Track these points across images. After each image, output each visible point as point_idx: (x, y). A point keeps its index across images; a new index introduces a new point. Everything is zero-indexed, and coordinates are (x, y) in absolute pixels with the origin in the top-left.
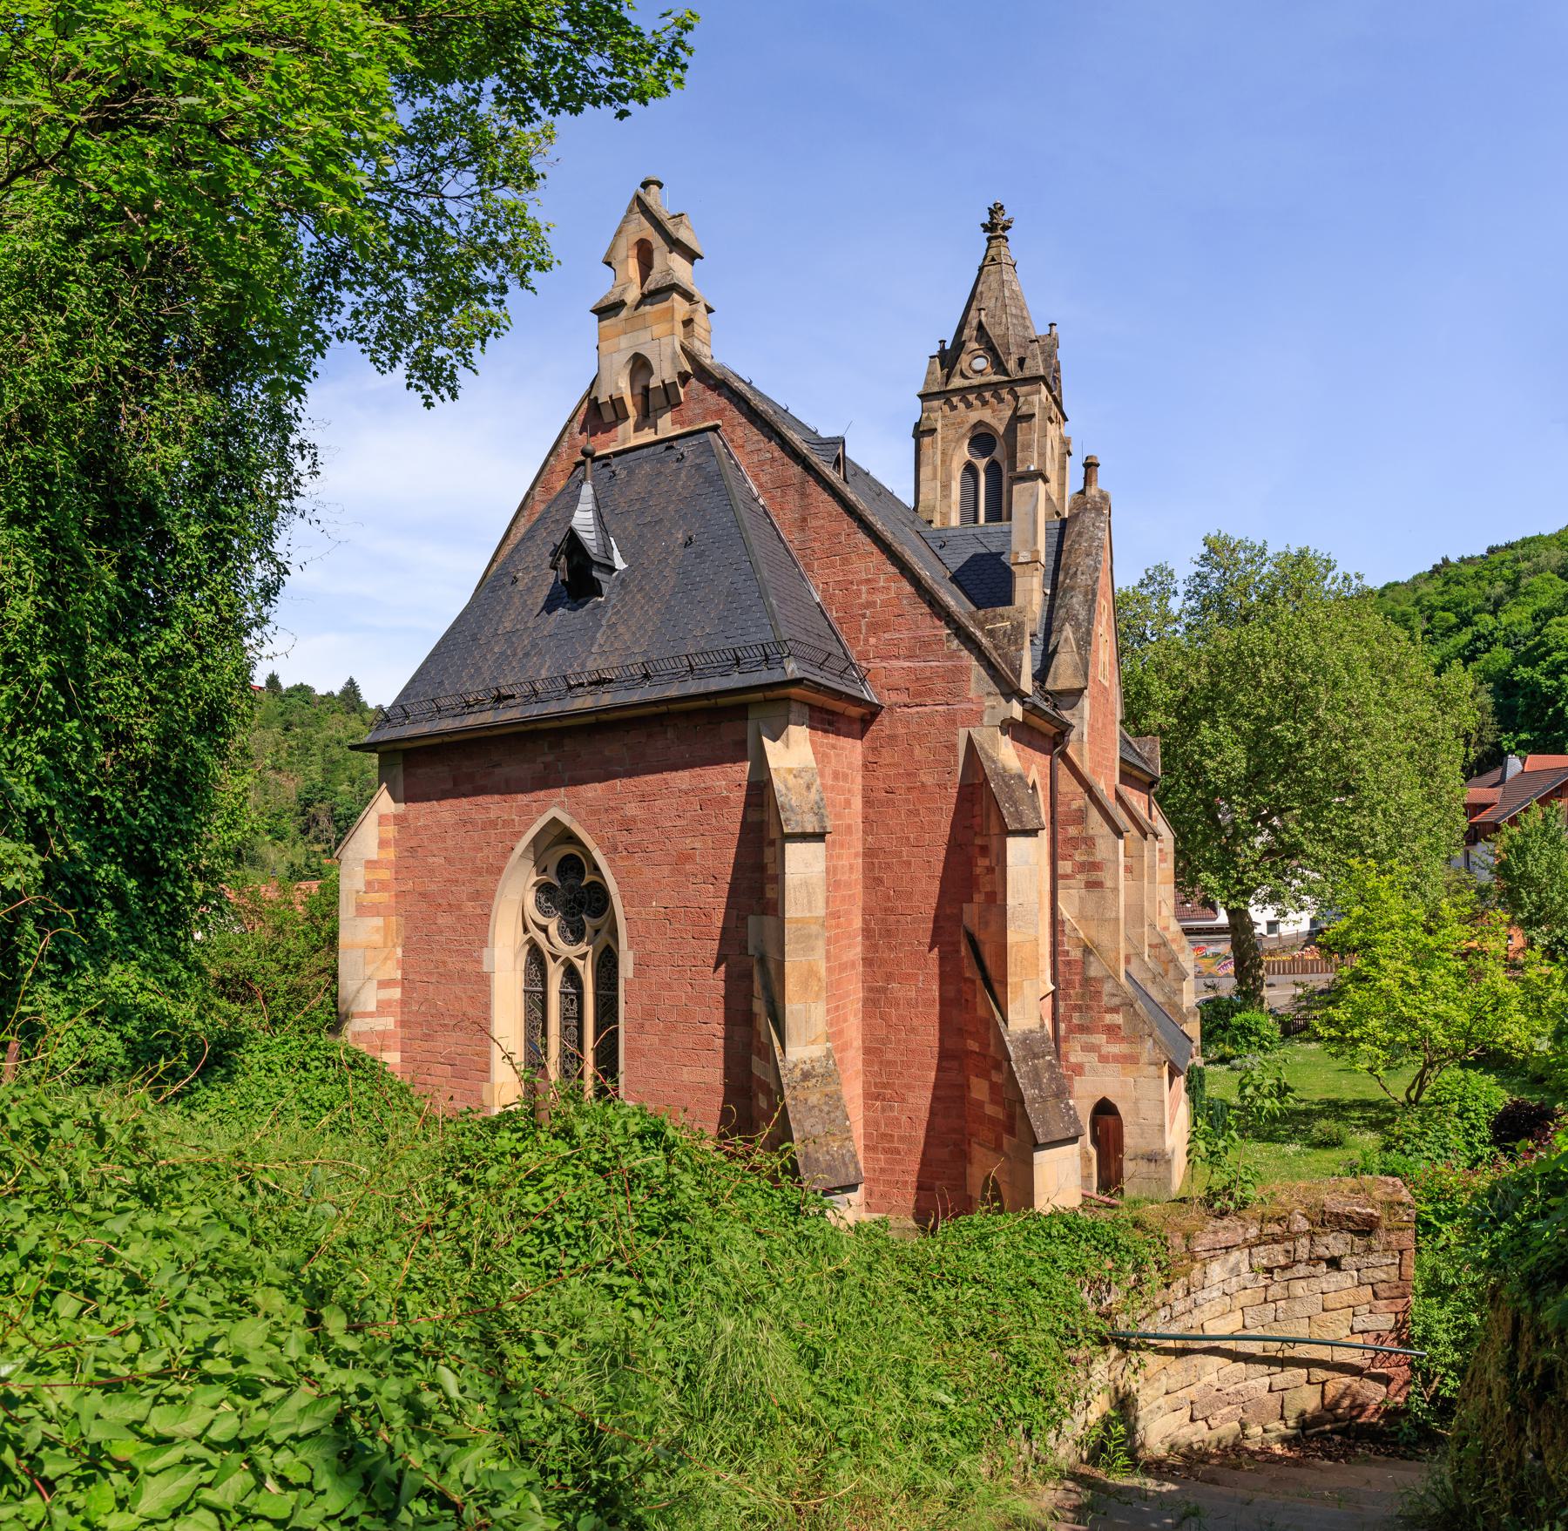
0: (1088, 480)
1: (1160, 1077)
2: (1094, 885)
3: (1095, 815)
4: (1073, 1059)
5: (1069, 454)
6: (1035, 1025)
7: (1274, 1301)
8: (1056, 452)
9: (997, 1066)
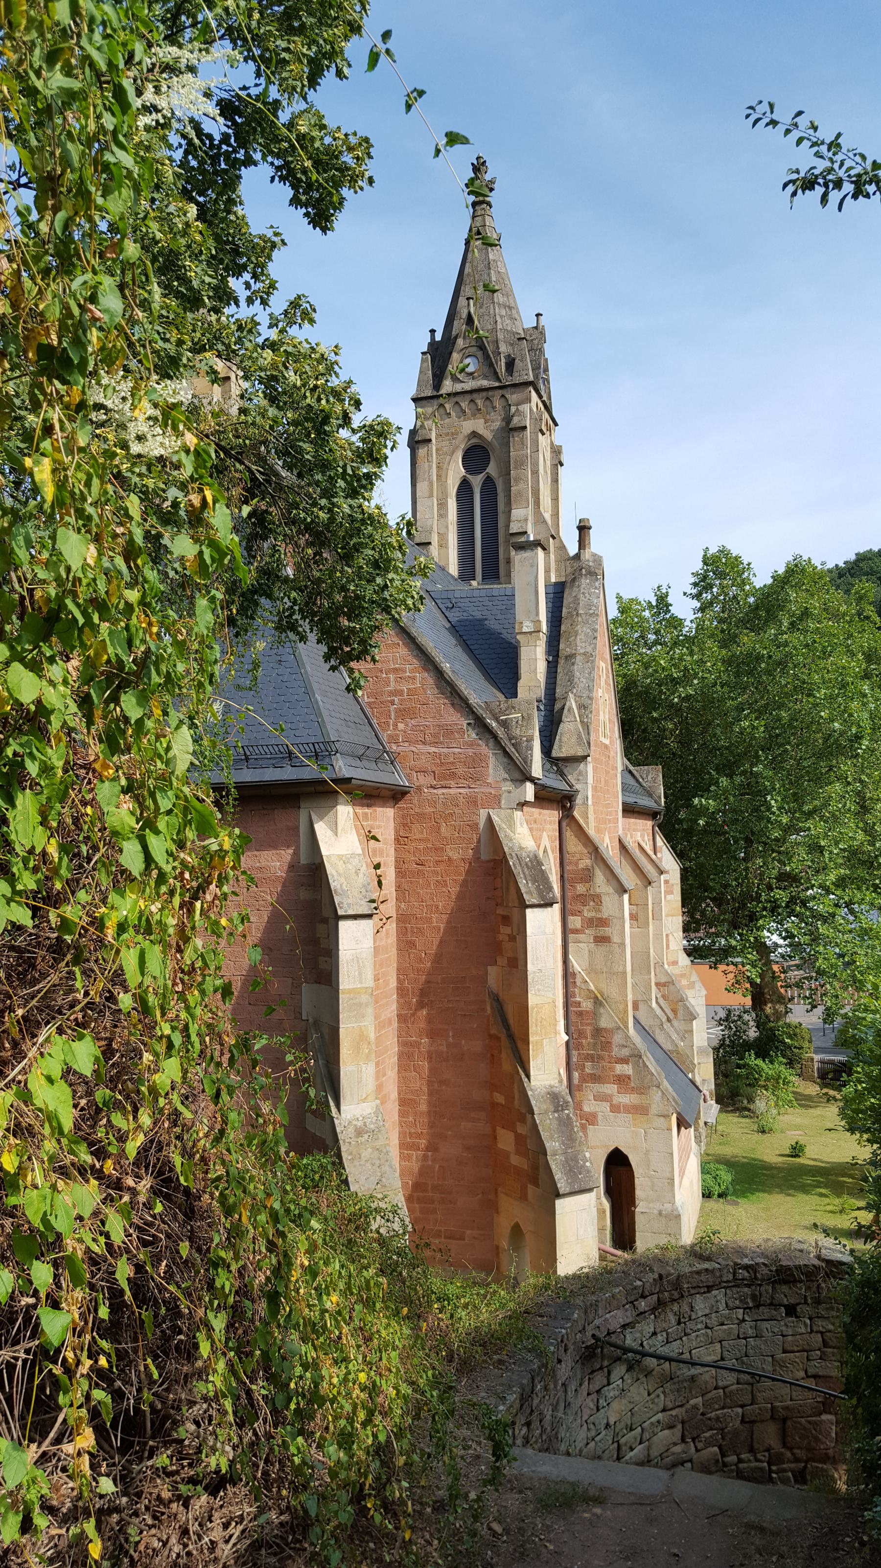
0: (583, 542)
1: (670, 1129)
2: (602, 940)
3: (600, 877)
4: (586, 1108)
5: (562, 465)
6: (555, 1082)
7: (745, 1338)
8: (548, 463)
9: (522, 1119)
